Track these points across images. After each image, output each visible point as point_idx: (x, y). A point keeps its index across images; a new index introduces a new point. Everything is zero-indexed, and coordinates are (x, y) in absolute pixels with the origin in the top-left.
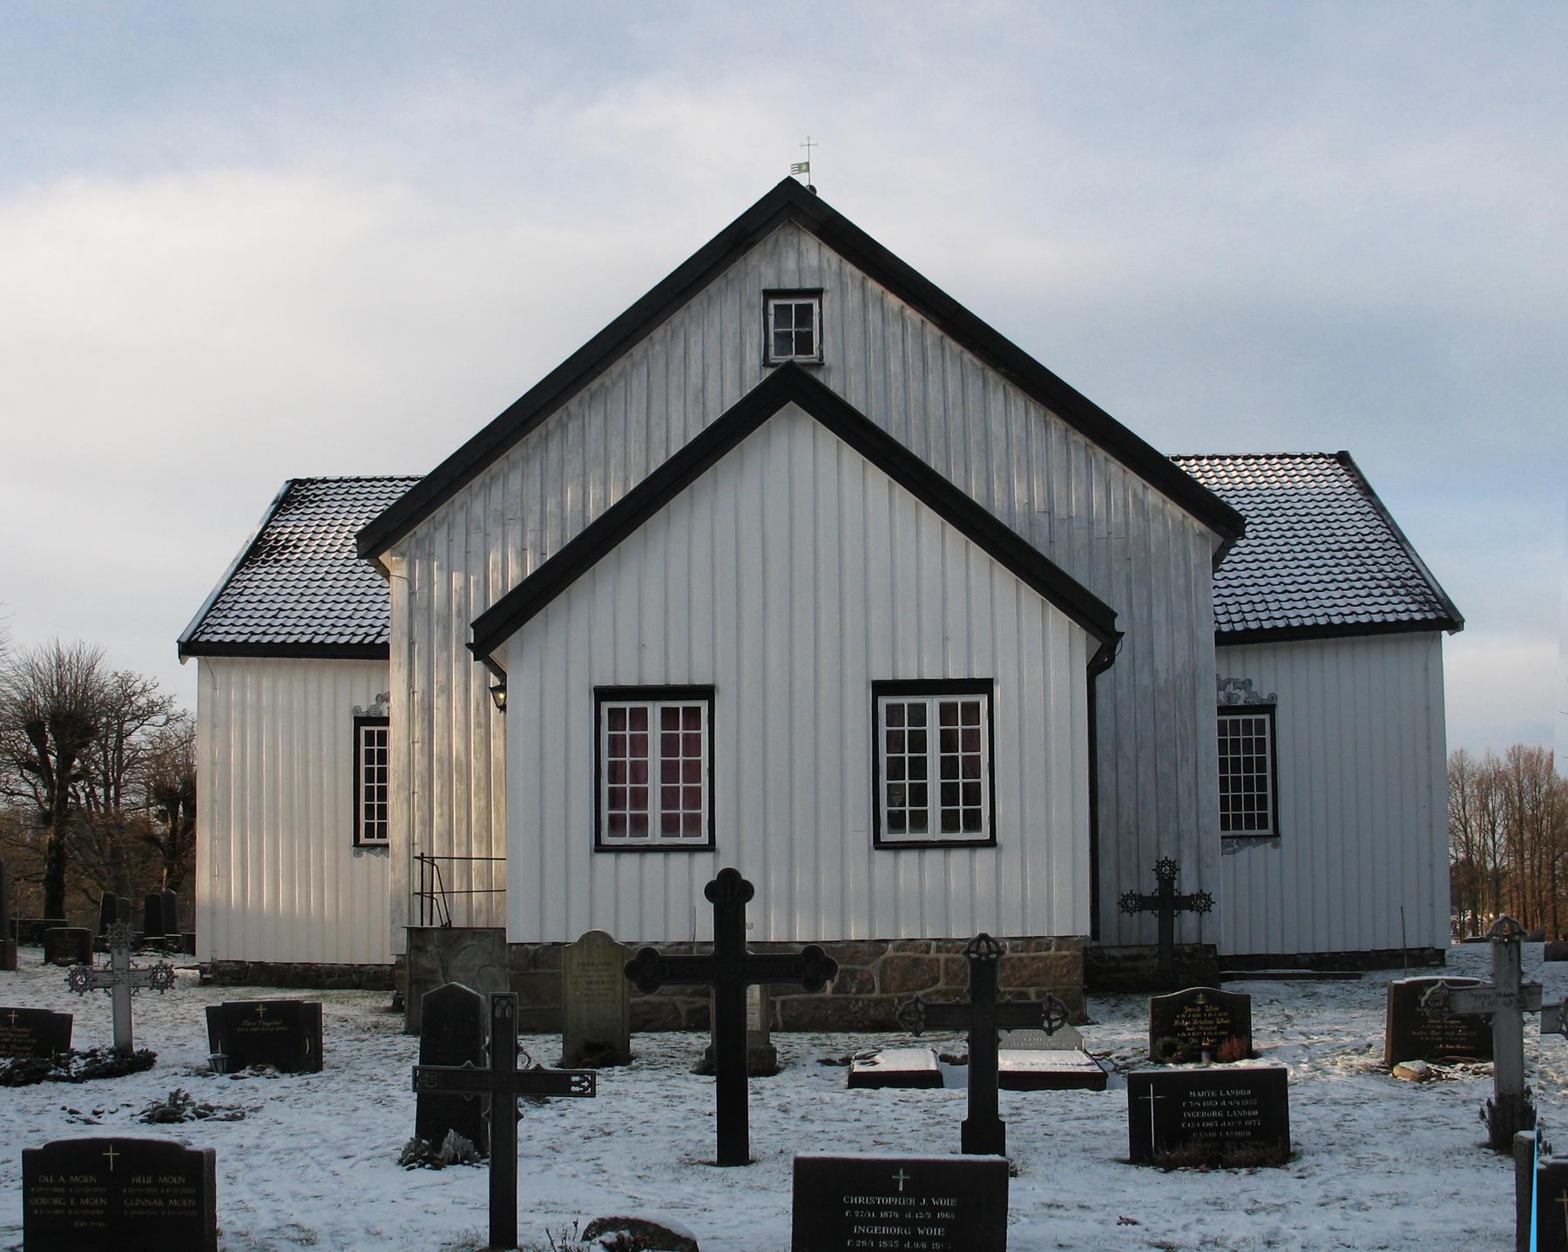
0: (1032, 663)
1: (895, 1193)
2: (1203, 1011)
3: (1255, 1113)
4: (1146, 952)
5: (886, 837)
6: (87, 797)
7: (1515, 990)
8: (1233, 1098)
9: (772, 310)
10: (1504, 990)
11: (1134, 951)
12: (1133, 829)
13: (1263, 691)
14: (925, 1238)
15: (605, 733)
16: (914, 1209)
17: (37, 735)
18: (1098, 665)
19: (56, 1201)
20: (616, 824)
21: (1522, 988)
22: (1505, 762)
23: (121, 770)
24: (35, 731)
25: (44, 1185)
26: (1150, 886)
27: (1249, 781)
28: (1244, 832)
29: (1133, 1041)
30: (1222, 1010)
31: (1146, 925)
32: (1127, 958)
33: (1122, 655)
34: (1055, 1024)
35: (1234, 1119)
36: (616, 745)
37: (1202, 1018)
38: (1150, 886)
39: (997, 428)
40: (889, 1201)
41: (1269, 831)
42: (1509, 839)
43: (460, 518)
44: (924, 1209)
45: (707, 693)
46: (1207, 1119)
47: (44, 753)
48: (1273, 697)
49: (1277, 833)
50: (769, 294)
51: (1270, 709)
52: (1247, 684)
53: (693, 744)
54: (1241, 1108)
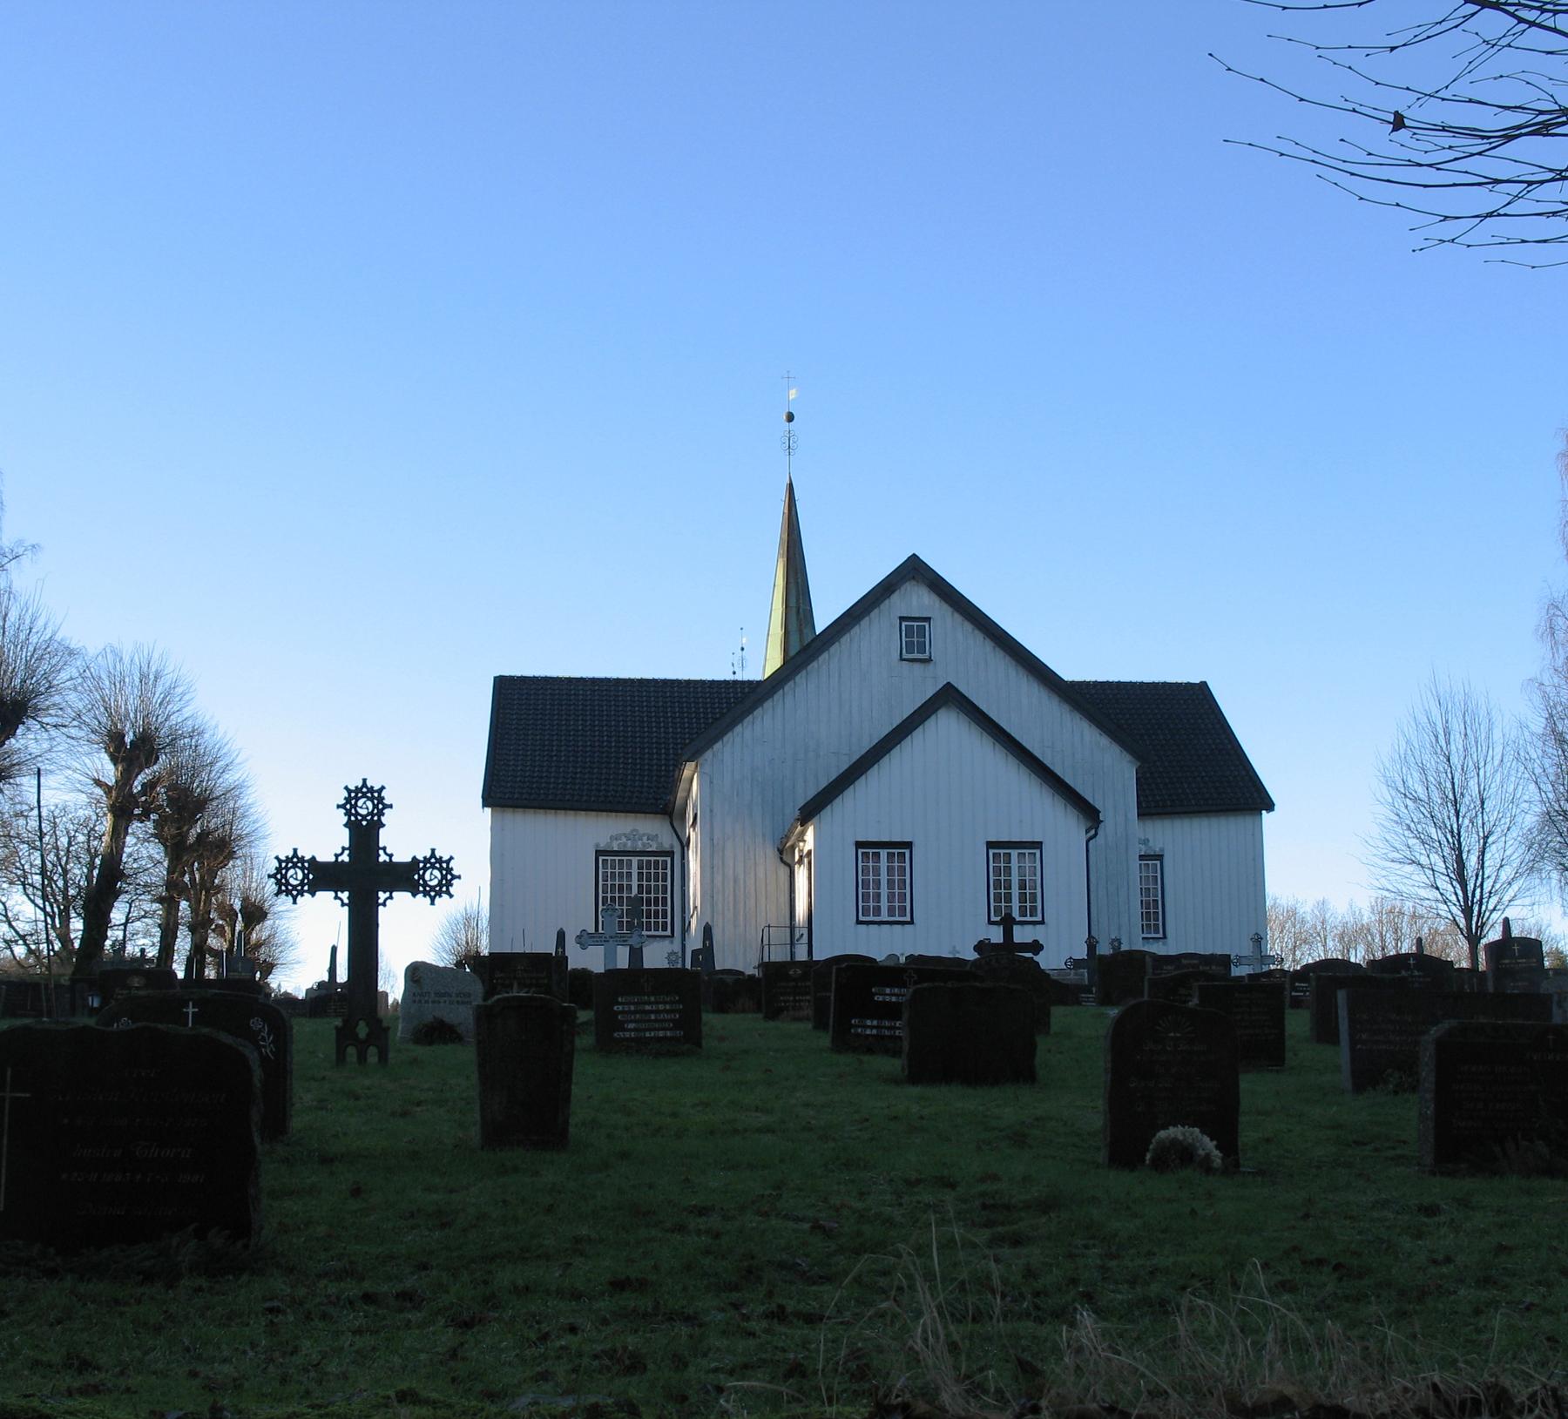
20: (866, 912)
29: (983, 1194)
45: (909, 845)
49: (1165, 937)
50: (902, 619)
51: (1160, 857)
53: (997, 871)
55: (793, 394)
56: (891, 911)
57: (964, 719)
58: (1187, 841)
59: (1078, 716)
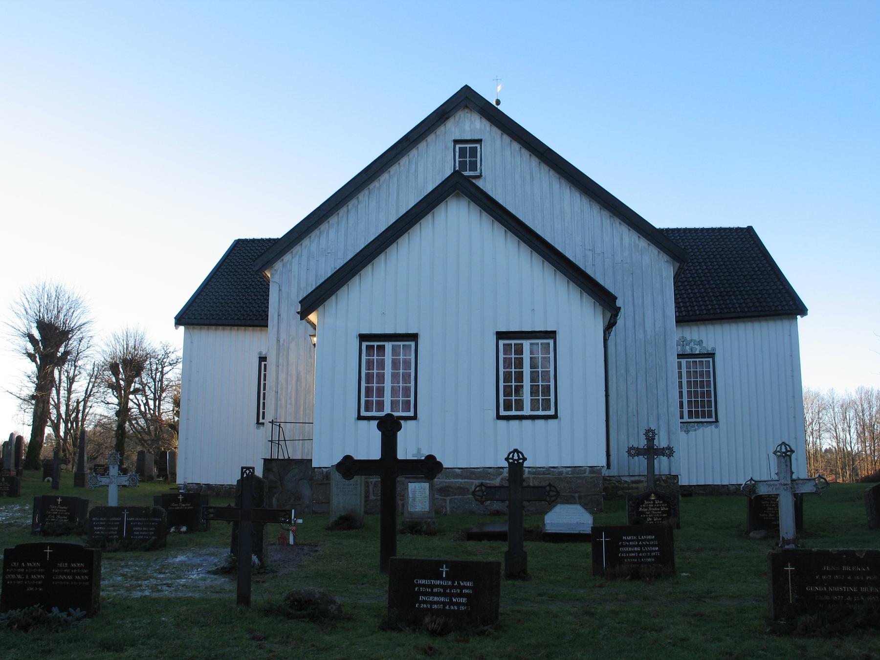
1: (441, 578)
2: (654, 503)
3: (657, 549)
4: (642, 479)
5: (502, 413)
6: (145, 405)
7: (789, 482)
8: (646, 540)
9: (457, 150)
10: (783, 481)
11: (637, 478)
12: (635, 414)
13: (708, 346)
14: (457, 604)
15: (364, 358)
16: (452, 587)
17: (116, 373)
18: (609, 327)
19: (19, 577)
20: (508, 407)
21: (793, 480)
22: (855, 396)
23: (163, 390)
24: (114, 368)
25: (13, 568)
26: (642, 443)
27: (703, 393)
28: (700, 420)
30: (664, 503)
31: (640, 464)
32: (633, 482)
33: (620, 322)
34: (553, 499)
35: (646, 552)
36: (370, 364)
37: (654, 507)
38: (642, 443)
40: (438, 582)
41: (713, 419)
42: (859, 436)
43: (305, 253)
44: (456, 587)
46: (632, 552)
47: (118, 380)
48: (714, 349)
49: (717, 421)
50: (456, 142)
51: (712, 355)
52: (700, 343)
54: (649, 546)
55: (499, 88)
56: (534, 406)
57: (475, 210)
58: (733, 345)
59: (617, 221)
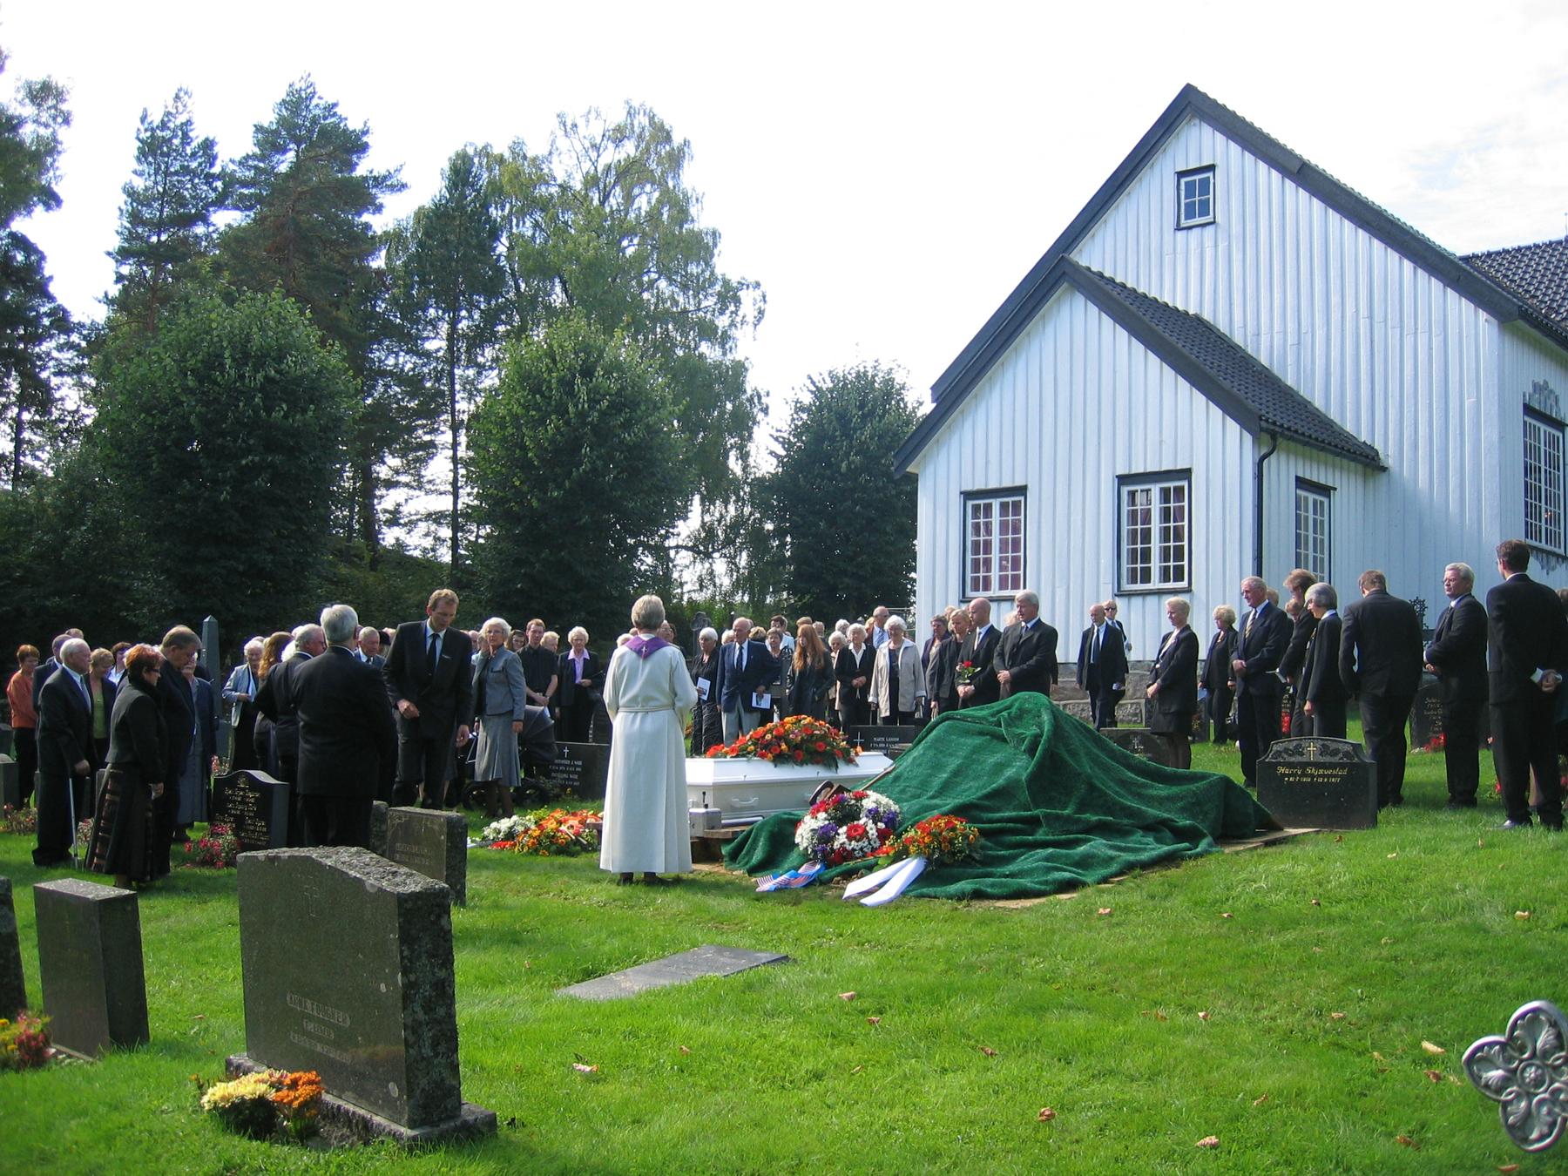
0: (1212, 445)
5: (1127, 587)
9: (1183, 187)
39: (1167, 248)
